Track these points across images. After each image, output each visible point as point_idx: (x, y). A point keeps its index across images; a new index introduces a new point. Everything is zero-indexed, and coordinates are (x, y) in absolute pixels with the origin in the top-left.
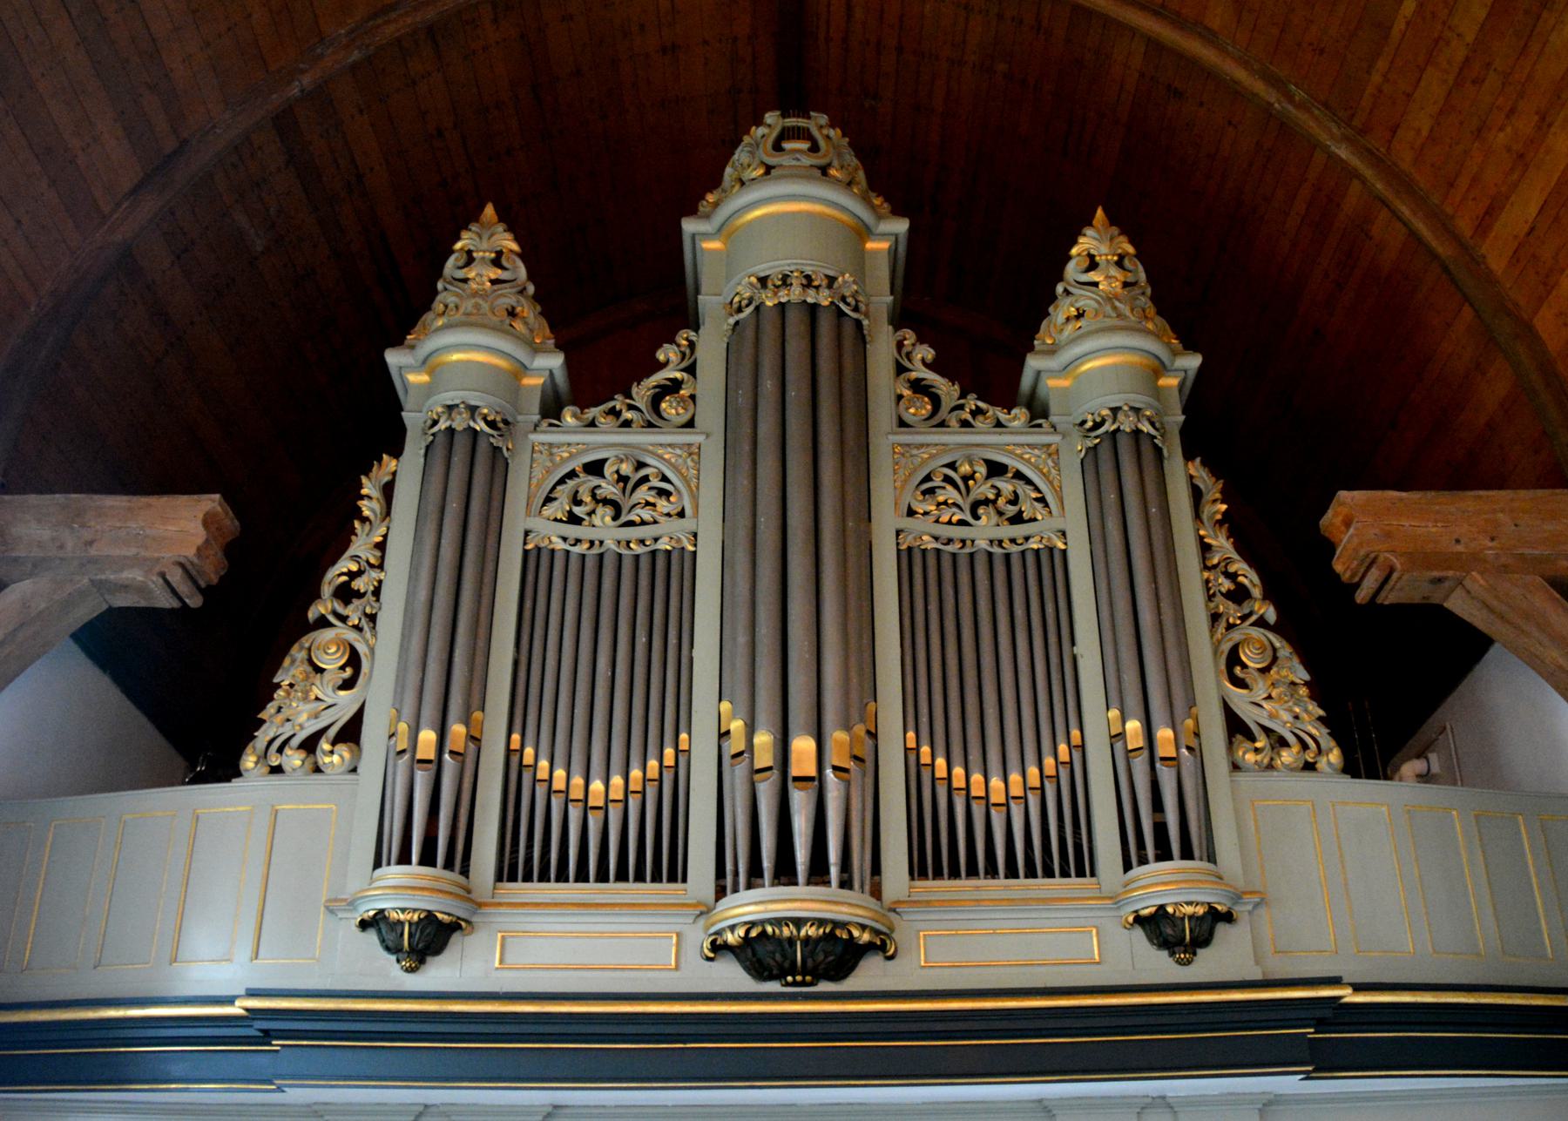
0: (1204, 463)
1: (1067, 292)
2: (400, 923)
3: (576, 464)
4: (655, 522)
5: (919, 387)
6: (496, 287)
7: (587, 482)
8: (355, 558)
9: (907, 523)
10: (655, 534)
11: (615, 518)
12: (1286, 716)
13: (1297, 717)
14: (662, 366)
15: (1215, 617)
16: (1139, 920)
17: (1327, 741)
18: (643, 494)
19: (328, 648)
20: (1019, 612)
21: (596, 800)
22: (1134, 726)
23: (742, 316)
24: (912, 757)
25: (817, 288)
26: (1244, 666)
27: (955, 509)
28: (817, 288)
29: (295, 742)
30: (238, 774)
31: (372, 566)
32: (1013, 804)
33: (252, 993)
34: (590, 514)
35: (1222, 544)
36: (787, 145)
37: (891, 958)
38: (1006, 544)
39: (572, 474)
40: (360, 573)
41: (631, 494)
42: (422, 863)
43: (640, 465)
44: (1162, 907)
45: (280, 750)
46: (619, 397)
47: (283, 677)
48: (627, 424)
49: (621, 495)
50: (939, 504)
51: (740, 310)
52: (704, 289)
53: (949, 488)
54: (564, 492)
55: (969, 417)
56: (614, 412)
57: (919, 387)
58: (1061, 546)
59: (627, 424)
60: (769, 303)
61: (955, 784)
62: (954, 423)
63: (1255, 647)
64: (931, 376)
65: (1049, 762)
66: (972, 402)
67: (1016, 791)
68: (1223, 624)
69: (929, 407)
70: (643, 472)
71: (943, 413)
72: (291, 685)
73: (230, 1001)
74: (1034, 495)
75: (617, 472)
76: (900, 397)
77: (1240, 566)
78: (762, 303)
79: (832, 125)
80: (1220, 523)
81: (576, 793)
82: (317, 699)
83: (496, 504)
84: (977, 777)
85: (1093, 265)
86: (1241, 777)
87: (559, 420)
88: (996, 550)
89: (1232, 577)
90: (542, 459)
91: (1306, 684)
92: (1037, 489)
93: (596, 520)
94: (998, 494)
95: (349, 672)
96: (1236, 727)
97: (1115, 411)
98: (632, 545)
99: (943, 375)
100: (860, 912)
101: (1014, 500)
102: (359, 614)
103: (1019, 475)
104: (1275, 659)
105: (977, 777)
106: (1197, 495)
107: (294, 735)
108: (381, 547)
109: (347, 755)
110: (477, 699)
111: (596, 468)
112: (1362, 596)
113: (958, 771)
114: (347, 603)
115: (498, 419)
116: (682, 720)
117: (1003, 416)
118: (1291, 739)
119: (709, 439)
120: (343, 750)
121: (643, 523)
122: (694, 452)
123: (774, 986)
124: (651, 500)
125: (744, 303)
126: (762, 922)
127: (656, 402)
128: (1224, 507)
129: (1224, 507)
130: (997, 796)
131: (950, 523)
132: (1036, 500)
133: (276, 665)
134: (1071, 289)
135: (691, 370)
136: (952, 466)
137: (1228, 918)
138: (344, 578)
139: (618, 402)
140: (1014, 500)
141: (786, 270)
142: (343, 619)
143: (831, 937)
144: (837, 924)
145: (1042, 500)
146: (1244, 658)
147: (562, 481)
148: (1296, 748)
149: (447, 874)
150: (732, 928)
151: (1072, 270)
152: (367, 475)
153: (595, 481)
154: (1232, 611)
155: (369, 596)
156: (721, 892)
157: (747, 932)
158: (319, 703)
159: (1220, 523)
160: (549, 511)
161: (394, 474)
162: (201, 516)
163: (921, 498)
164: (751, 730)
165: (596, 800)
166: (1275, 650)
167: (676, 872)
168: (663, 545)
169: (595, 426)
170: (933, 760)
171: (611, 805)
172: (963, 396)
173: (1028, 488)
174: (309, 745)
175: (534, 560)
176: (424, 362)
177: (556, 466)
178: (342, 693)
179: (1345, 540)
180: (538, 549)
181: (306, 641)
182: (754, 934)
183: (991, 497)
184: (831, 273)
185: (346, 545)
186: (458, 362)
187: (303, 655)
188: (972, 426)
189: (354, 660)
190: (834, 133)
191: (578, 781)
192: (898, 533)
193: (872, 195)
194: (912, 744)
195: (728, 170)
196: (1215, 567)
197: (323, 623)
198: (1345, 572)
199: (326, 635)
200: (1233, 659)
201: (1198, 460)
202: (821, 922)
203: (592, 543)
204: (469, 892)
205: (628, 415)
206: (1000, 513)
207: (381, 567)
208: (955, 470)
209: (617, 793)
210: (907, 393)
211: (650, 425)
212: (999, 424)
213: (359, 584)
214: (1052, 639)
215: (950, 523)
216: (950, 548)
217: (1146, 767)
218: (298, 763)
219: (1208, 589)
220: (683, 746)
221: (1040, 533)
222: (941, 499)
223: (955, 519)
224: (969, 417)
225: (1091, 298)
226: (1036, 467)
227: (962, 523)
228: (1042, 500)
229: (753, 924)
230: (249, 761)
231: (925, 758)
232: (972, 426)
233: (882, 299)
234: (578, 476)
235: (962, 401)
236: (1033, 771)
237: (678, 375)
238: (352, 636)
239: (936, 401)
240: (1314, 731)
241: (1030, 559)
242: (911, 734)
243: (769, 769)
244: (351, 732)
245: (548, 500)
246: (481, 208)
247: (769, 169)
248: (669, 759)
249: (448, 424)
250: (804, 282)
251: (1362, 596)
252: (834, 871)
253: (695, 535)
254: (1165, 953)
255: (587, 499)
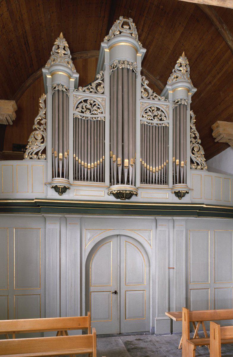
0: (193, 111)
1: (175, 71)
2: (60, 187)
3: (82, 100)
4: (97, 114)
5: (145, 90)
6: (65, 56)
7: (84, 104)
8: (40, 116)
10: (98, 116)
11: (90, 112)
12: (200, 160)
13: (201, 160)
14: (97, 79)
15: (191, 142)
16: (175, 193)
18: (95, 108)
19: (38, 134)
20: (160, 138)
21: (89, 167)
22: (178, 161)
23: (114, 69)
24: (75, 159)
25: (130, 65)
26: (194, 151)
27: (151, 117)
28: (130, 65)
29: (34, 153)
30: (24, 159)
31: (44, 118)
32: (156, 172)
33: (36, 199)
34: (85, 111)
35: (194, 127)
36: (125, 27)
38: (159, 125)
39: (81, 102)
40: (41, 120)
41: (93, 108)
44: (179, 191)
46: (89, 85)
47: (30, 140)
48: (91, 92)
49: (91, 108)
50: (148, 115)
51: (114, 68)
52: (105, 62)
53: (150, 112)
54: (80, 106)
55: (154, 98)
56: (88, 89)
57: (145, 90)
58: (168, 126)
59: (91, 92)
60: (120, 67)
61: (148, 168)
62: (151, 98)
63: (197, 147)
64: (148, 88)
65: (162, 165)
67: (157, 170)
68: (192, 143)
69: (147, 95)
70: (95, 103)
71: (149, 96)
72: (31, 142)
73: (33, 200)
74: (164, 115)
75: (90, 103)
76: (142, 92)
77: (196, 132)
78: (119, 67)
79: (133, 22)
80: (194, 124)
81: (86, 166)
82: (37, 145)
83: (68, 108)
84: (151, 167)
85: (181, 66)
87: (78, 89)
88: (157, 126)
89: (195, 134)
93: (87, 112)
94: (158, 115)
95: (42, 140)
96: (192, 162)
97: (181, 99)
98: (94, 119)
99: (150, 87)
101: (161, 116)
102: (43, 128)
103: (162, 111)
104: (199, 150)
106: (191, 117)
107: (33, 152)
108: (45, 114)
109: (44, 156)
111: (85, 101)
113: (148, 166)
115: (67, 89)
116: (104, 153)
117: (160, 98)
118: (200, 164)
119: (107, 96)
121: (95, 114)
123: (119, 200)
124: (96, 109)
125: (115, 66)
126: (120, 190)
127: (96, 87)
128: (195, 120)
129: (195, 120)
130: (154, 171)
131: (149, 119)
132: (164, 116)
133: (28, 138)
134: (176, 71)
135: (103, 80)
136: (150, 108)
137: (188, 193)
138: (38, 120)
139: (89, 87)
141: (124, 60)
143: (130, 193)
144: (131, 191)
145: (165, 116)
146: (195, 149)
147: (79, 104)
148: (200, 166)
150: (115, 191)
151: (177, 66)
152: (40, 98)
153: (85, 104)
154: (194, 140)
155: (44, 125)
156: (111, 185)
157: (117, 192)
158: (37, 146)
159: (194, 124)
160: (77, 110)
161: (46, 98)
162: (11, 105)
163: (145, 114)
164: (117, 157)
165: (89, 167)
166: (200, 148)
167: (103, 180)
168: (99, 119)
169: (85, 92)
170: (144, 164)
171: (92, 168)
172: (153, 93)
173: (163, 114)
174: (37, 154)
175: (76, 120)
176: (51, 73)
178: (42, 144)
179: (216, 130)
180: (76, 118)
181: (33, 133)
182: (118, 192)
183: (157, 115)
184: (132, 62)
185: (38, 114)
186: (61, 74)
187: (33, 136)
188: (154, 99)
189: (43, 138)
190: (134, 24)
191: (86, 163)
192: (141, 120)
193: (139, 42)
194: (75, 156)
195: (110, 31)
196: (192, 132)
197: (36, 129)
198: (214, 136)
199: (37, 132)
200: (193, 149)
201: (192, 110)
202: (129, 191)
203: (86, 117)
204: (69, 182)
205: (91, 90)
206: (158, 118)
208: (151, 109)
209: (93, 166)
210: (143, 91)
211: (96, 93)
212: (159, 100)
213: (42, 122)
214: (165, 144)
215: (149, 119)
216: (149, 125)
217: (179, 168)
218: (36, 157)
219: (191, 136)
220: (104, 158)
221: (165, 123)
222: (148, 114)
223: (150, 119)
224: (154, 98)
225: (180, 74)
226: (165, 110)
227: (152, 120)
228: (165, 116)
229: (118, 190)
231: (143, 163)
232: (154, 99)
233: (139, 69)
234: (82, 103)
235: (153, 94)
236: (160, 167)
237: (101, 82)
238: (42, 133)
239: (148, 94)
240: (204, 163)
241: (162, 128)
242: (75, 155)
243: (121, 164)
244: (44, 152)
245: (77, 107)
246: (60, 34)
247: (120, 33)
248: (101, 161)
249: (58, 89)
250: (127, 63)
252: (130, 182)
253: (105, 118)
254: (177, 198)
255: (84, 108)
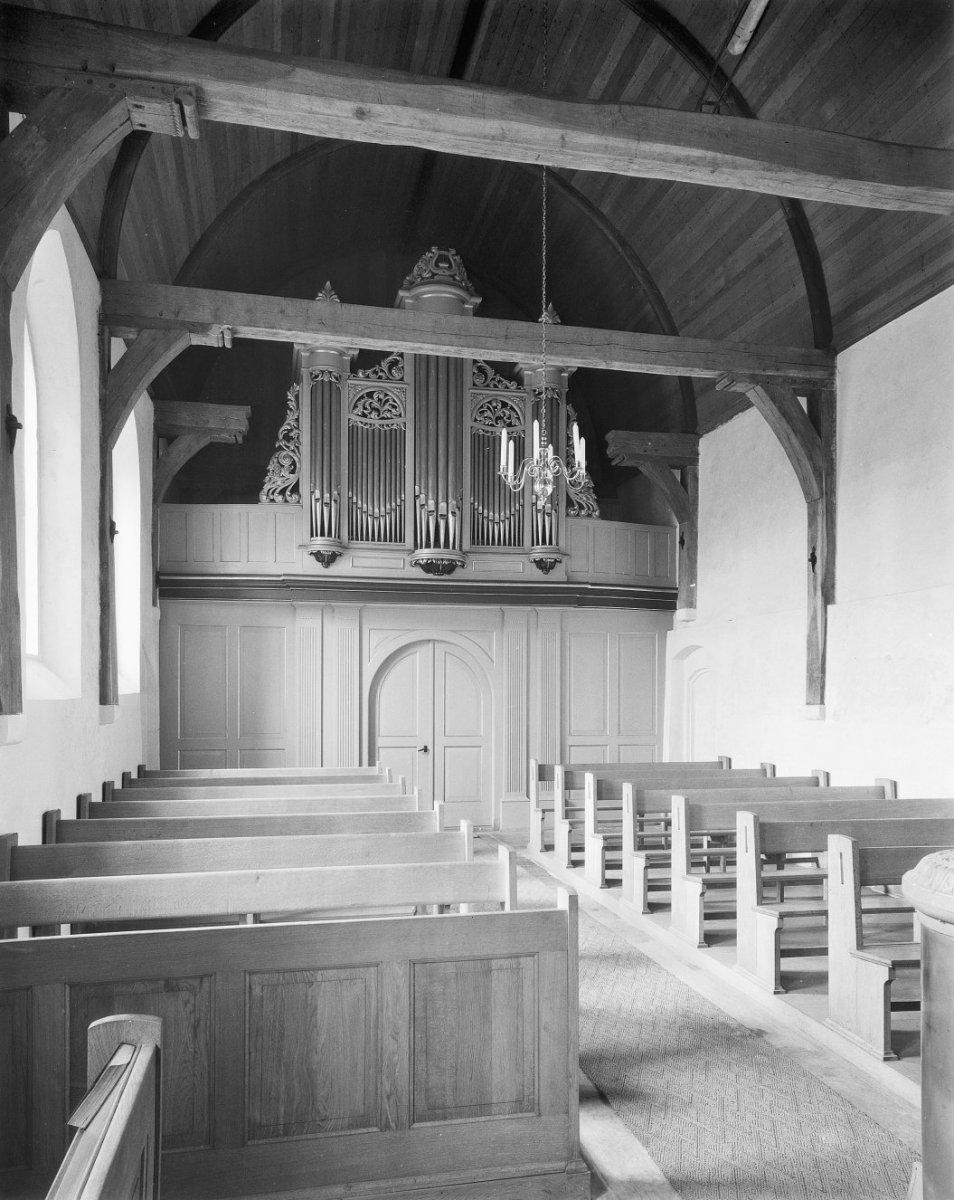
8: (289, 424)
9: (474, 424)
17: (596, 507)
18: (387, 407)
29: (278, 491)
37: (463, 566)
39: (362, 397)
40: (291, 430)
42: (445, 547)
43: (386, 395)
45: (273, 493)
47: (270, 467)
48: (380, 377)
56: (375, 372)
59: (380, 377)
65: (513, 509)
66: (498, 378)
84: (491, 513)
86: (569, 519)
90: (352, 392)
91: (593, 488)
92: (517, 414)
100: (355, 546)
101: (509, 418)
103: (512, 408)
105: (491, 513)
108: (297, 420)
110: (339, 483)
111: (370, 395)
112: (614, 464)
114: (289, 442)
120: (295, 496)
121: (388, 418)
122: (404, 391)
123: (431, 576)
137: (560, 562)
139: (377, 368)
140: (509, 418)
142: (288, 447)
147: (359, 400)
149: (437, 550)
168: (394, 427)
174: (282, 492)
175: (352, 430)
177: (358, 393)
197: (280, 448)
202: (449, 560)
205: (380, 374)
206: (505, 422)
207: (297, 428)
211: (388, 378)
212: (507, 387)
213: (292, 434)
228: (518, 418)
230: (263, 498)
238: (292, 454)
244: (296, 489)
251: (614, 464)
